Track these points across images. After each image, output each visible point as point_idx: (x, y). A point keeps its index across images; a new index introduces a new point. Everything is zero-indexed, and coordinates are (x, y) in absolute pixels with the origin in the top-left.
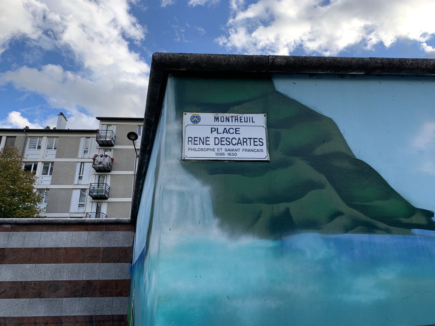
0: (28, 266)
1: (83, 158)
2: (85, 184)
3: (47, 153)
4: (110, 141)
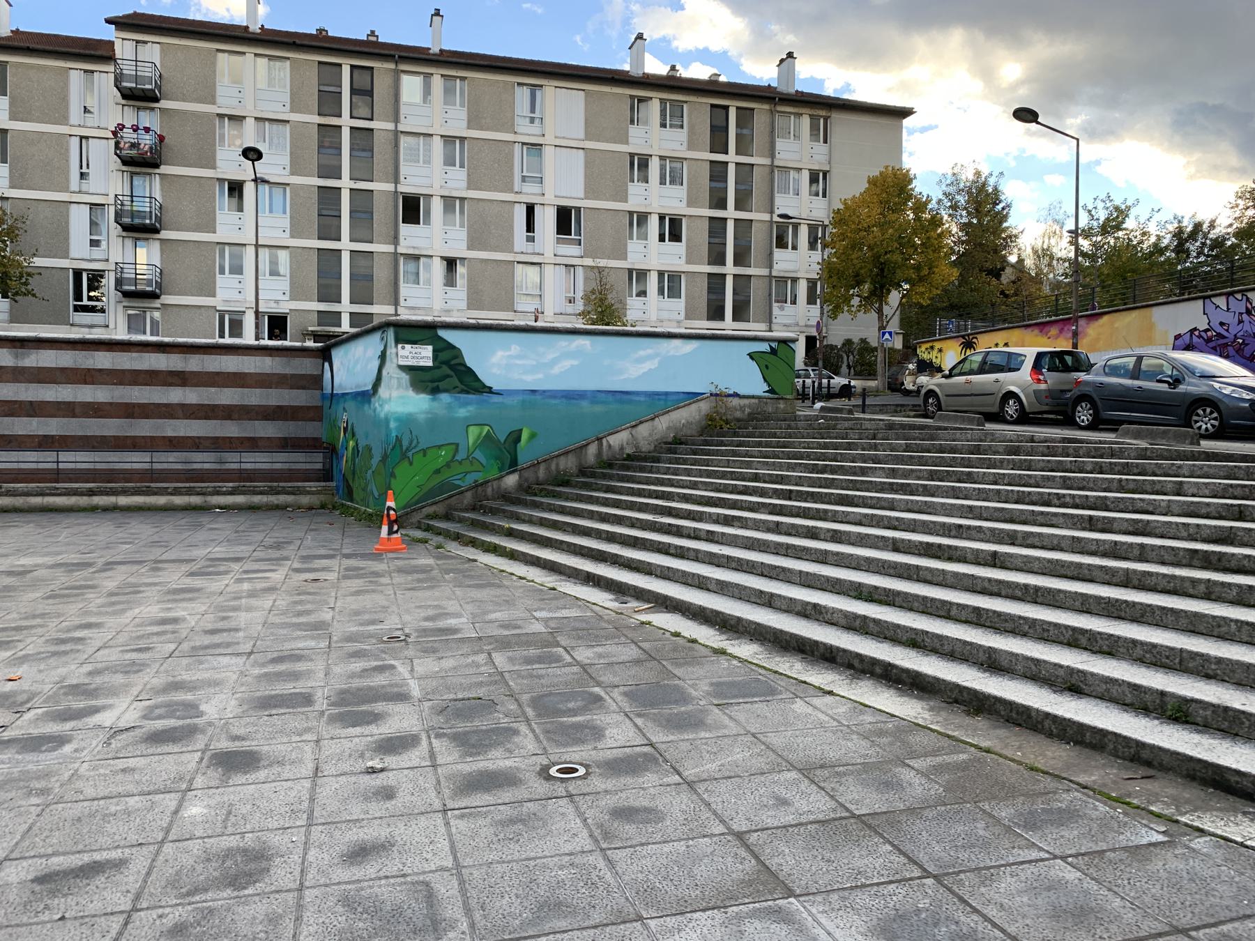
0: (213, 390)
2: (99, 192)
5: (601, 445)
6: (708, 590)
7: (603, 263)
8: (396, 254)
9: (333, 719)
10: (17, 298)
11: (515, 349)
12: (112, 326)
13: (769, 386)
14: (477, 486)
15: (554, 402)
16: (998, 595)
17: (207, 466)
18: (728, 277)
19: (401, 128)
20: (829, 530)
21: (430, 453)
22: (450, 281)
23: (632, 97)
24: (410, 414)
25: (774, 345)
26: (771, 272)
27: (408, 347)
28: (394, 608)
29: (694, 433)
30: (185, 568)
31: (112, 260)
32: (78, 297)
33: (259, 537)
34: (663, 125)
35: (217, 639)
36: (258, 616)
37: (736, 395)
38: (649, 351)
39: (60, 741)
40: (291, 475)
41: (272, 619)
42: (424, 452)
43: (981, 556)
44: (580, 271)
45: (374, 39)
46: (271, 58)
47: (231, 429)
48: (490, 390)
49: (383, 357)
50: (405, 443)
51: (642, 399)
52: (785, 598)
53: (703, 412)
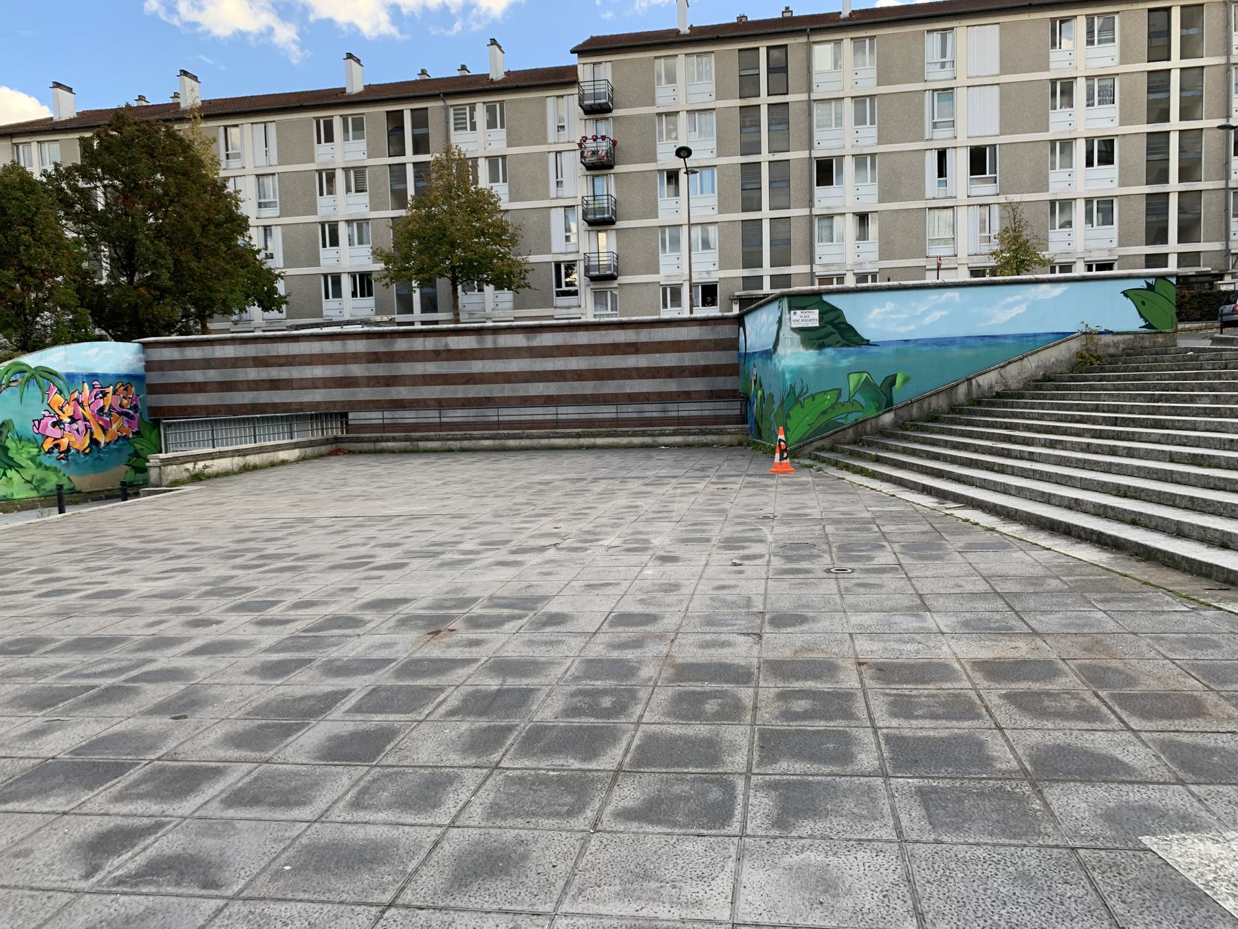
0: (657, 355)
1: (558, 143)
3: (490, 138)
4: (607, 103)
5: (970, 385)
6: (1010, 494)
7: (1016, 198)
8: (811, 216)
9: (719, 548)
10: (519, 290)
11: (889, 306)
12: (583, 306)
13: (1146, 321)
14: (857, 424)
15: (925, 349)
16: (1224, 490)
17: (655, 415)
18: (1171, 196)
19: (814, 97)
20: (1125, 448)
21: (819, 399)
22: (863, 235)
23: (1053, 20)
24: (802, 367)
25: (1150, 281)
26: (1227, 184)
27: (799, 312)
28: (773, 504)
29: (1064, 370)
30: (641, 481)
31: (582, 252)
32: (559, 285)
33: (691, 464)
34: (1090, 42)
35: (660, 515)
36: (686, 506)
37: (1107, 332)
38: (1017, 297)
39: (586, 549)
40: (716, 420)
41: (693, 507)
42: (813, 397)
43: (1231, 462)
44: (996, 210)
45: (788, 15)
46: (699, 55)
47: (672, 386)
48: (868, 343)
49: (780, 321)
50: (798, 391)
51: (1010, 341)
52: (1058, 496)
53: (1074, 351)
